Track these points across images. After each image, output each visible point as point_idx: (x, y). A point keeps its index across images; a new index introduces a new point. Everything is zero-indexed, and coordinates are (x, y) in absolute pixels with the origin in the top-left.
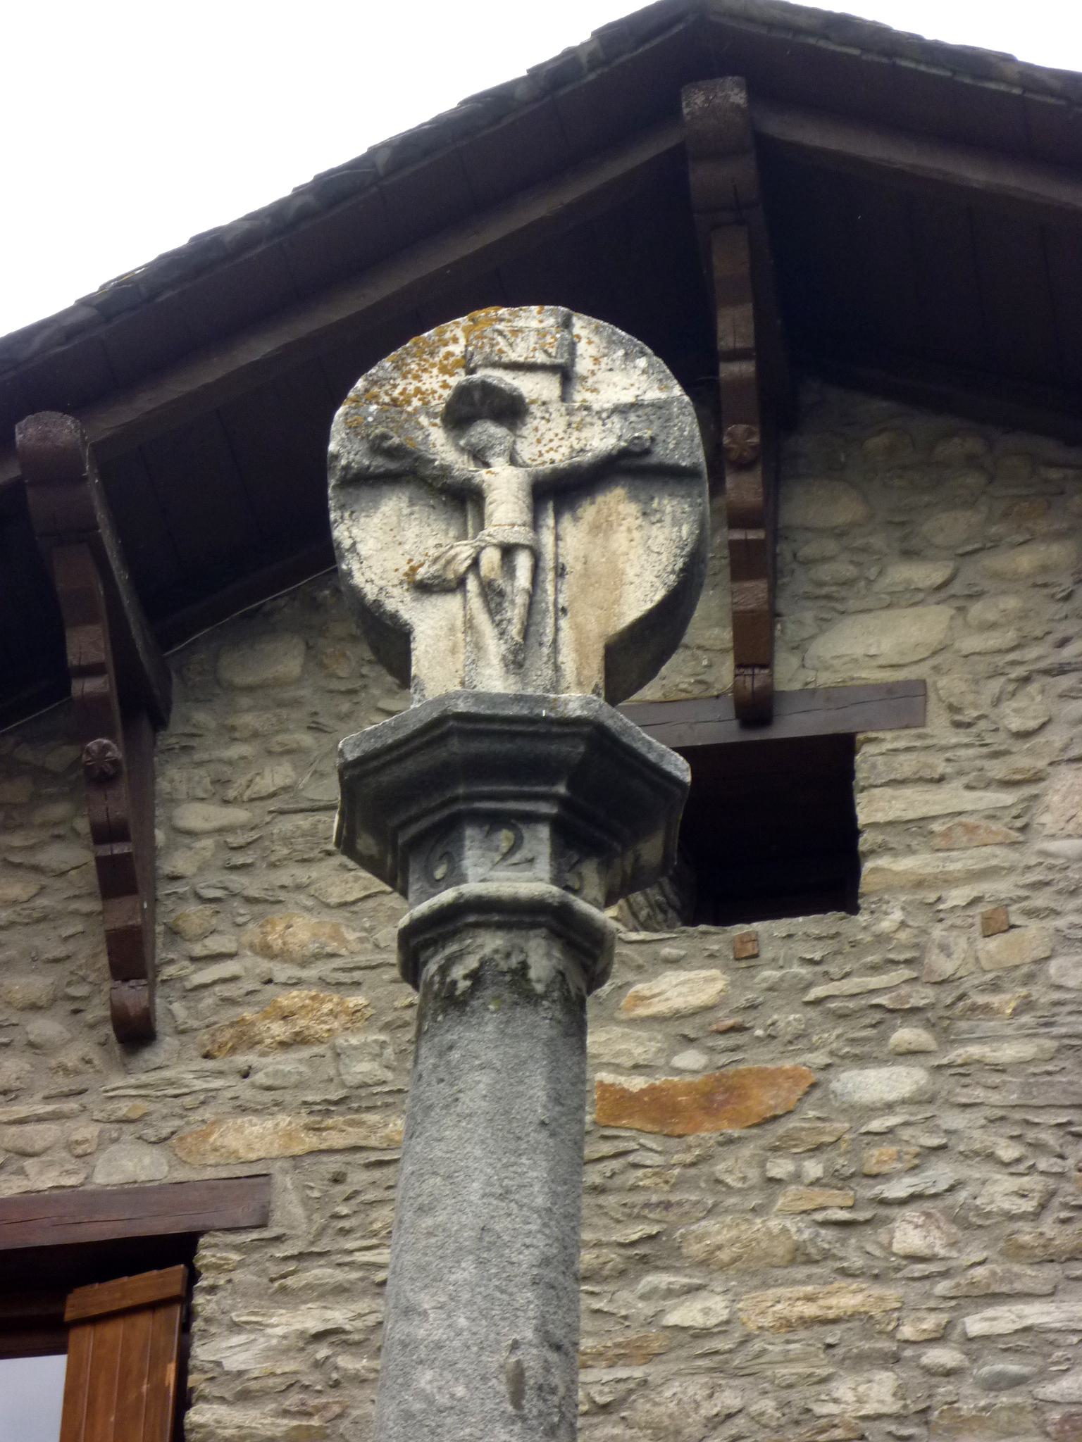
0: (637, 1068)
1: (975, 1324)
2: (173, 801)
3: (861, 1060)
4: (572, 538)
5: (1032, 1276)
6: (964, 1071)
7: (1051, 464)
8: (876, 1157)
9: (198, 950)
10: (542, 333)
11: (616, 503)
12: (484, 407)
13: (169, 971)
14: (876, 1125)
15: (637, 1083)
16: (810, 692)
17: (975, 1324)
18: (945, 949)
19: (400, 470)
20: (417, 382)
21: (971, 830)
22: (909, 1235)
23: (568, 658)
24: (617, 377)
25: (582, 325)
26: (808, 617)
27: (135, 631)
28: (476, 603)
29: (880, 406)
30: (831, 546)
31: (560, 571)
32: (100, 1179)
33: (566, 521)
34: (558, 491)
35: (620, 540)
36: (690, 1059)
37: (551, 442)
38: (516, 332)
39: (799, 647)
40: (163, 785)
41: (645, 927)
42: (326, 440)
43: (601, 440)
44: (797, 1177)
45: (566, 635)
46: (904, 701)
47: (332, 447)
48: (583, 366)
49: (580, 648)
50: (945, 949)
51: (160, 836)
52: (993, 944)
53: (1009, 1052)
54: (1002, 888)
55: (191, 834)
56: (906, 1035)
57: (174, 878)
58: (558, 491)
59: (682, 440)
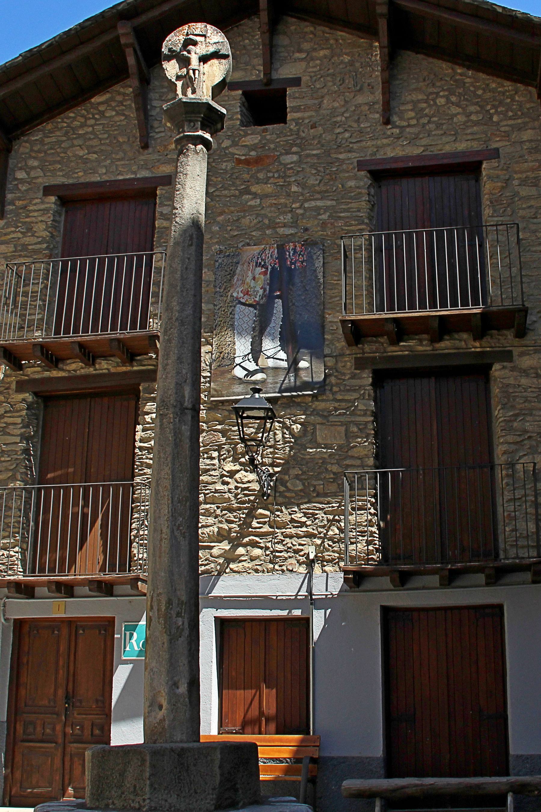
0: (243, 155)
1: (306, 205)
2: (151, 100)
3: (287, 153)
4: (206, 68)
5: (318, 196)
6: (308, 156)
7: (327, 33)
8: (289, 172)
9: (157, 130)
10: (201, 28)
11: (215, 62)
12: (189, 43)
13: (151, 135)
14: (289, 166)
15: (243, 158)
16: (278, 79)
17: (306, 205)
18: (303, 132)
19: (173, 55)
20: (174, 40)
21: (309, 108)
22: (294, 188)
23: (205, 91)
24: (215, 37)
25: (209, 26)
26: (278, 63)
27: (143, 65)
28: (188, 80)
29: (294, 20)
30: (283, 49)
31: (204, 74)
32: (138, 176)
33: (205, 65)
34: (204, 59)
35: (215, 68)
36: (253, 153)
37: (201, 49)
38: (197, 28)
39: (277, 70)
40: (149, 96)
41: (246, 126)
42: (162, 48)
43: (212, 49)
44: (273, 177)
45: (205, 87)
46: (296, 82)
47: (163, 50)
48: (208, 35)
49: (207, 88)
50: (303, 132)
51: (149, 107)
52: (312, 131)
53: (315, 152)
54: (314, 119)
55: (155, 107)
56: (295, 149)
57: (152, 116)
58: (204, 59)
59: (226, 49)
